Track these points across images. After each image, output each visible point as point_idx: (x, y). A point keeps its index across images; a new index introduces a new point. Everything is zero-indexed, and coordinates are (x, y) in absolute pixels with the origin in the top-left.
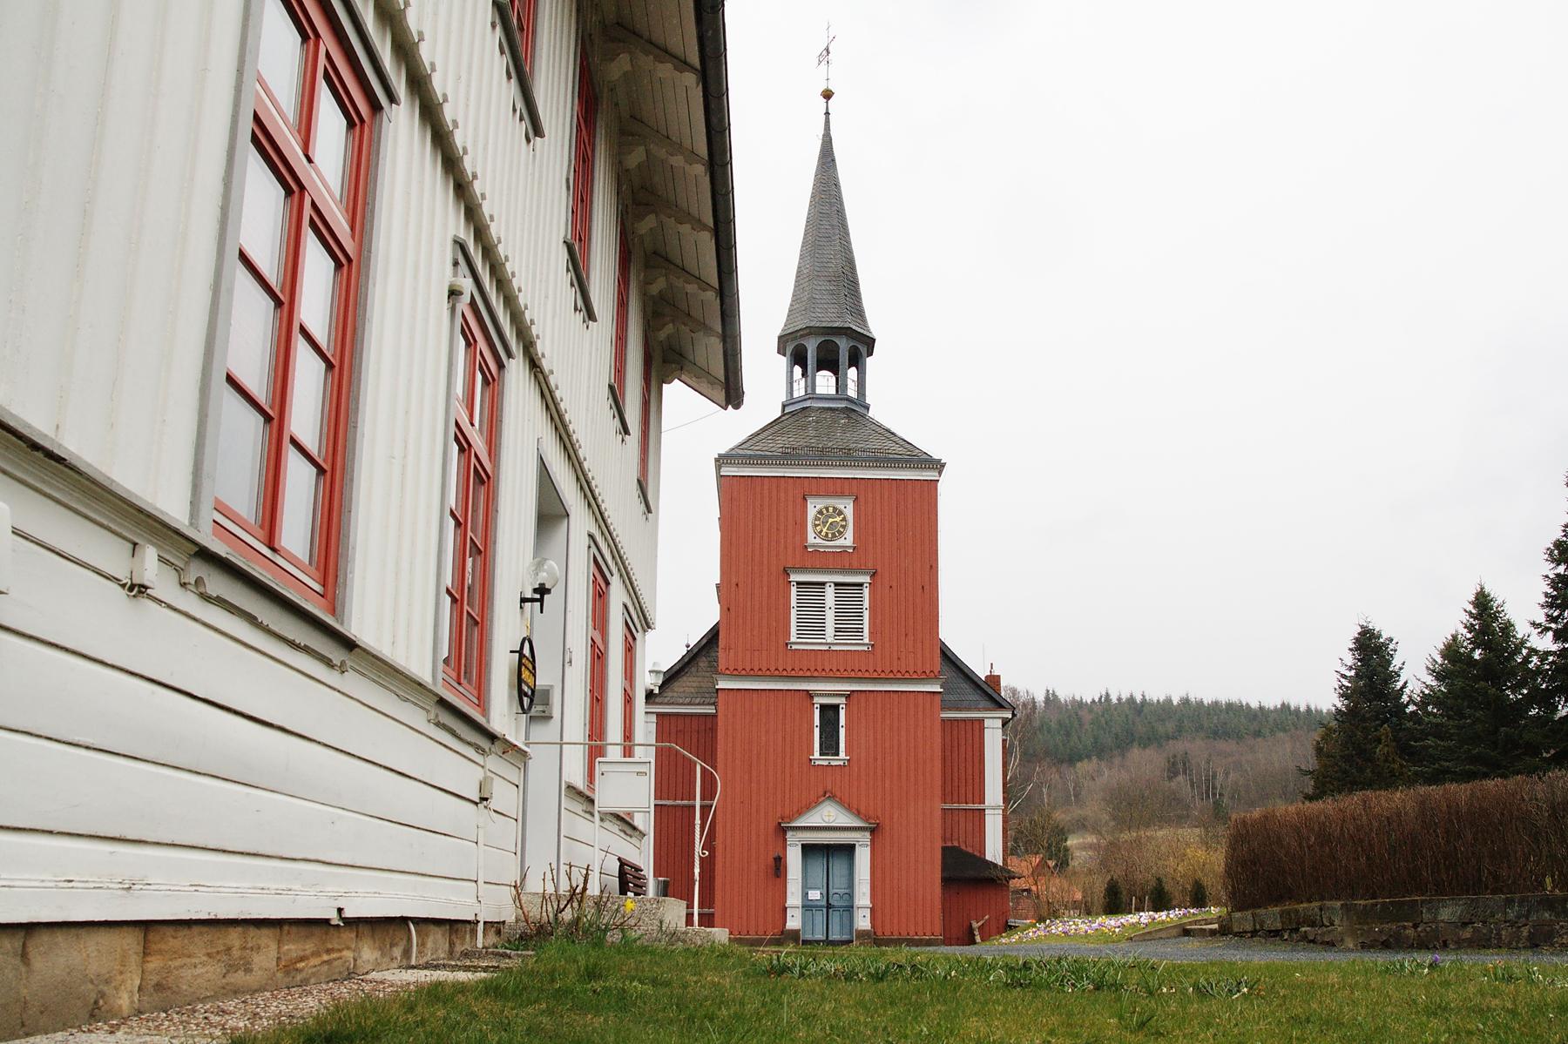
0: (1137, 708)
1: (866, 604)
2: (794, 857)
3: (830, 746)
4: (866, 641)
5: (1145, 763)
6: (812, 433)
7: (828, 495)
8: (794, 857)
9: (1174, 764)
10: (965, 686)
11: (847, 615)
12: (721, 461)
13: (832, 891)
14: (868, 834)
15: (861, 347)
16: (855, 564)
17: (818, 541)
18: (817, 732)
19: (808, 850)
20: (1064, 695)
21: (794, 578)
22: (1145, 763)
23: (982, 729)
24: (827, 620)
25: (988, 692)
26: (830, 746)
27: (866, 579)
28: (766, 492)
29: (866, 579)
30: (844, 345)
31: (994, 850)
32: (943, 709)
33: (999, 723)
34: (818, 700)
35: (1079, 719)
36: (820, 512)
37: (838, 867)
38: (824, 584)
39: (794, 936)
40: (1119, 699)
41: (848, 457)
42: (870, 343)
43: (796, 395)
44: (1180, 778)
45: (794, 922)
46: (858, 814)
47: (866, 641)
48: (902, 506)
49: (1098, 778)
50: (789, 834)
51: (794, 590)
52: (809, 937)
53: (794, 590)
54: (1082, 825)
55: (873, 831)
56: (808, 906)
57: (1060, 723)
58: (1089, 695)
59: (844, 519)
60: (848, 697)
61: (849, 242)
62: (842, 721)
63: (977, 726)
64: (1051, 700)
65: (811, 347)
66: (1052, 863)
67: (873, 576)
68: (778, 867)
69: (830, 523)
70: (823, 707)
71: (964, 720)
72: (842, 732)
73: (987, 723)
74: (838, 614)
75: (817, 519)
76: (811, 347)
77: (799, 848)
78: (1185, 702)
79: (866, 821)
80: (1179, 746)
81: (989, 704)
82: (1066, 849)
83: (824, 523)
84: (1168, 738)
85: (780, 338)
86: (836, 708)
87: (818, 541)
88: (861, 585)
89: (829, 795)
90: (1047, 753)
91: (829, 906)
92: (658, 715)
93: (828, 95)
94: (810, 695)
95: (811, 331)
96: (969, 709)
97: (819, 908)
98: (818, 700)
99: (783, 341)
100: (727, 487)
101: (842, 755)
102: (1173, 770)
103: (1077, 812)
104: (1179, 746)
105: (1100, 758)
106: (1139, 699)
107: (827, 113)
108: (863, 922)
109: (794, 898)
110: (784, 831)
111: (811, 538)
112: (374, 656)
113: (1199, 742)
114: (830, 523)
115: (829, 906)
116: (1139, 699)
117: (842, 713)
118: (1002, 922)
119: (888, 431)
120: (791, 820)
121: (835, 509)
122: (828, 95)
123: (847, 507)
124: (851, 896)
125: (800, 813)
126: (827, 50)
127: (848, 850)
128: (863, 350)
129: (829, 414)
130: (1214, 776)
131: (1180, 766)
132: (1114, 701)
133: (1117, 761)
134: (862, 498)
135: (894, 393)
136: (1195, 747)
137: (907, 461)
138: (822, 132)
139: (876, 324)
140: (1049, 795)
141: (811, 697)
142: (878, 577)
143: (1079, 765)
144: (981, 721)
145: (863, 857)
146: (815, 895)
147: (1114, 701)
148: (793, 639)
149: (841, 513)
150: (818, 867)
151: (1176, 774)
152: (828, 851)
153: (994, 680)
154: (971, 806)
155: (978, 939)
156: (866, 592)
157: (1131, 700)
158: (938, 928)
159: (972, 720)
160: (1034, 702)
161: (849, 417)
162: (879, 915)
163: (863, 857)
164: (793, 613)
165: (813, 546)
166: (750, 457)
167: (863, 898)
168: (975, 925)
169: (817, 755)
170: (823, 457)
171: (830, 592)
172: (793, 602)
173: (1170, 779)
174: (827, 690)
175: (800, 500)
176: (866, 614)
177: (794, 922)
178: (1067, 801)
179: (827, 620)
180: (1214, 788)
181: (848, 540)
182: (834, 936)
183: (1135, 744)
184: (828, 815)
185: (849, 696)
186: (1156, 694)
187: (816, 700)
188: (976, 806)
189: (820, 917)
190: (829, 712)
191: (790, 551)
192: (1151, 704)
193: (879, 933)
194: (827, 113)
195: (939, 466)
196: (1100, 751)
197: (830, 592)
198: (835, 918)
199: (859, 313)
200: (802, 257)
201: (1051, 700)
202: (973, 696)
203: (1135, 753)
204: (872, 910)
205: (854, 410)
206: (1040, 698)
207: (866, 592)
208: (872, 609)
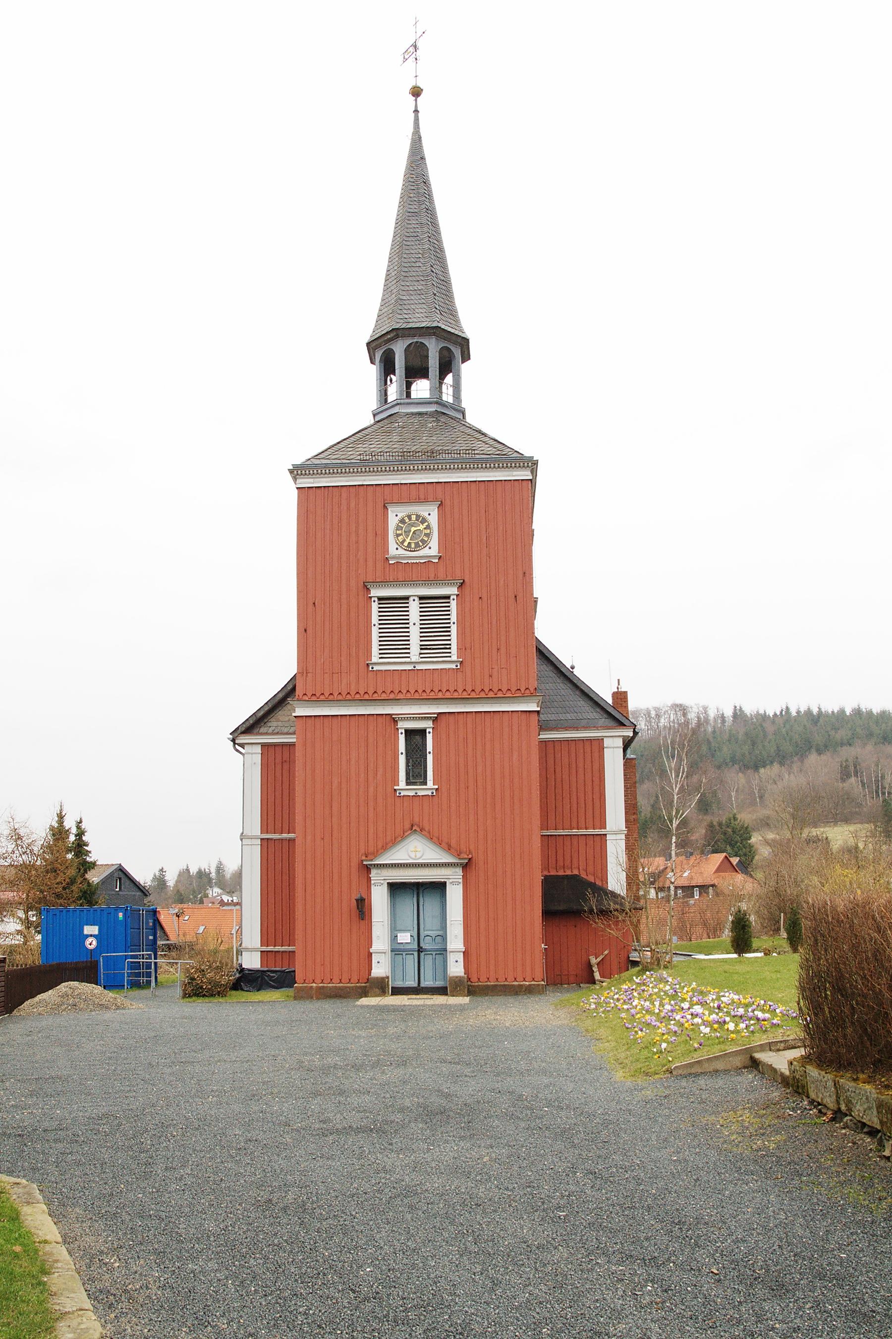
0: (814, 719)
1: (454, 618)
2: (379, 898)
3: (416, 774)
4: (454, 658)
5: (819, 769)
6: (396, 438)
7: (410, 502)
8: (379, 898)
9: (847, 767)
10: (582, 703)
11: (434, 633)
12: (296, 472)
13: (422, 935)
14: (459, 871)
15: (454, 350)
16: (441, 575)
17: (401, 552)
18: (402, 760)
19: (395, 888)
20: (749, 709)
21: (376, 592)
22: (819, 769)
23: (602, 748)
24: (411, 640)
25: (615, 713)
26: (416, 774)
27: (452, 591)
28: (344, 502)
29: (452, 591)
30: (433, 347)
31: (616, 880)
32: (291, 745)
33: (620, 743)
34: (403, 725)
35: (764, 730)
36: (402, 521)
37: (430, 905)
38: (407, 598)
39: (381, 986)
40: (798, 712)
41: (431, 459)
42: (464, 344)
43: (390, 399)
44: (853, 780)
45: (380, 968)
46: (449, 848)
47: (454, 658)
48: (494, 509)
49: (782, 780)
50: (374, 873)
51: (375, 606)
52: (399, 984)
53: (375, 606)
54: (765, 823)
55: (465, 867)
56: (397, 951)
57: (746, 734)
58: (772, 708)
59: (428, 527)
60: (435, 720)
61: (439, 241)
62: (430, 747)
63: (595, 744)
64: (738, 714)
65: (399, 349)
66: (735, 860)
67: (461, 586)
68: (362, 908)
69: (413, 532)
70: (409, 733)
71: (568, 741)
72: (430, 758)
73: (607, 742)
74: (424, 630)
75: (398, 528)
76: (399, 349)
77: (385, 888)
78: (858, 712)
79: (458, 855)
80: (848, 753)
81: (612, 723)
82: (751, 846)
83: (407, 532)
84: (842, 744)
85: (368, 344)
86: (422, 732)
87: (401, 552)
88: (448, 597)
89: (414, 828)
90: (734, 761)
91: (420, 950)
92: (263, 745)
93: (416, 92)
94: (393, 720)
95: (397, 334)
96: (586, 728)
97: (409, 952)
98: (403, 725)
99: (372, 346)
100: (312, 504)
101: (430, 783)
102: (845, 774)
103: (762, 813)
104: (848, 753)
105: (782, 764)
106: (815, 711)
107: (416, 111)
108: (456, 968)
109: (380, 942)
110: (368, 869)
111: (393, 549)
112: (582, 691)
113: (869, 747)
114: (413, 532)
115: (420, 950)
116: (815, 711)
117: (429, 738)
118: (623, 959)
119: (479, 432)
120: (376, 854)
121: (418, 517)
122: (416, 92)
123: (431, 514)
124: (444, 938)
125: (386, 847)
126: (415, 47)
127: (440, 887)
128: (457, 352)
129: (416, 420)
130: (883, 777)
131: (852, 768)
132: (794, 714)
133: (795, 767)
134: (447, 503)
135: (490, 396)
136: (865, 753)
137: (495, 461)
138: (410, 129)
139: (471, 322)
140: (736, 799)
141: (395, 721)
142: (467, 588)
143: (762, 770)
144: (600, 741)
145: (455, 895)
146: (405, 938)
147: (794, 714)
148: (375, 659)
149: (424, 521)
150: (408, 905)
151: (848, 776)
152: (418, 889)
153: (621, 697)
154: (591, 831)
155: (597, 976)
156: (453, 604)
157: (809, 712)
158: (539, 972)
159: (590, 740)
160: (723, 717)
161: (438, 421)
162: (473, 958)
163: (455, 895)
164: (375, 632)
165: (394, 558)
166: (326, 466)
167: (456, 941)
168: (594, 961)
169: (402, 784)
170: (405, 461)
171: (414, 607)
172: (375, 619)
173: (843, 780)
174: (412, 713)
175: (380, 505)
176: (454, 629)
177: (380, 968)
178: (753, 803)
179: (411, 640)
180: (883, 788)
181: (432, 549)
182: (427, 983)
183: (813, 750)
184: (416, 854)
185: (437, 719)
186: (831, 706)
187: (401, 725)
188: (597, 831)
189: (411, 962)
190: (415, 737)
191: (370, 563)
192: (827, 715)
193: (474, 978)
194: (416, 111)
195: (532, 464)
196: (782, 758)
197: (414, 607)
198: (428, 962)
199: (452, 313)
200: (391, 260)
201: (738, 714)
202: (593, 714)
203: (813, 758)
204: (465, 953)
205: (448, 415)
206: (729, 713)
207: (453, 604)
208: (460, 622)
